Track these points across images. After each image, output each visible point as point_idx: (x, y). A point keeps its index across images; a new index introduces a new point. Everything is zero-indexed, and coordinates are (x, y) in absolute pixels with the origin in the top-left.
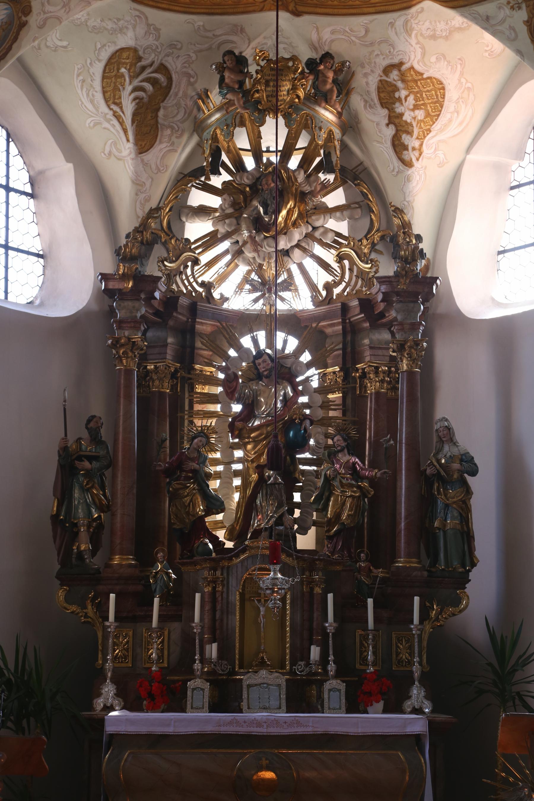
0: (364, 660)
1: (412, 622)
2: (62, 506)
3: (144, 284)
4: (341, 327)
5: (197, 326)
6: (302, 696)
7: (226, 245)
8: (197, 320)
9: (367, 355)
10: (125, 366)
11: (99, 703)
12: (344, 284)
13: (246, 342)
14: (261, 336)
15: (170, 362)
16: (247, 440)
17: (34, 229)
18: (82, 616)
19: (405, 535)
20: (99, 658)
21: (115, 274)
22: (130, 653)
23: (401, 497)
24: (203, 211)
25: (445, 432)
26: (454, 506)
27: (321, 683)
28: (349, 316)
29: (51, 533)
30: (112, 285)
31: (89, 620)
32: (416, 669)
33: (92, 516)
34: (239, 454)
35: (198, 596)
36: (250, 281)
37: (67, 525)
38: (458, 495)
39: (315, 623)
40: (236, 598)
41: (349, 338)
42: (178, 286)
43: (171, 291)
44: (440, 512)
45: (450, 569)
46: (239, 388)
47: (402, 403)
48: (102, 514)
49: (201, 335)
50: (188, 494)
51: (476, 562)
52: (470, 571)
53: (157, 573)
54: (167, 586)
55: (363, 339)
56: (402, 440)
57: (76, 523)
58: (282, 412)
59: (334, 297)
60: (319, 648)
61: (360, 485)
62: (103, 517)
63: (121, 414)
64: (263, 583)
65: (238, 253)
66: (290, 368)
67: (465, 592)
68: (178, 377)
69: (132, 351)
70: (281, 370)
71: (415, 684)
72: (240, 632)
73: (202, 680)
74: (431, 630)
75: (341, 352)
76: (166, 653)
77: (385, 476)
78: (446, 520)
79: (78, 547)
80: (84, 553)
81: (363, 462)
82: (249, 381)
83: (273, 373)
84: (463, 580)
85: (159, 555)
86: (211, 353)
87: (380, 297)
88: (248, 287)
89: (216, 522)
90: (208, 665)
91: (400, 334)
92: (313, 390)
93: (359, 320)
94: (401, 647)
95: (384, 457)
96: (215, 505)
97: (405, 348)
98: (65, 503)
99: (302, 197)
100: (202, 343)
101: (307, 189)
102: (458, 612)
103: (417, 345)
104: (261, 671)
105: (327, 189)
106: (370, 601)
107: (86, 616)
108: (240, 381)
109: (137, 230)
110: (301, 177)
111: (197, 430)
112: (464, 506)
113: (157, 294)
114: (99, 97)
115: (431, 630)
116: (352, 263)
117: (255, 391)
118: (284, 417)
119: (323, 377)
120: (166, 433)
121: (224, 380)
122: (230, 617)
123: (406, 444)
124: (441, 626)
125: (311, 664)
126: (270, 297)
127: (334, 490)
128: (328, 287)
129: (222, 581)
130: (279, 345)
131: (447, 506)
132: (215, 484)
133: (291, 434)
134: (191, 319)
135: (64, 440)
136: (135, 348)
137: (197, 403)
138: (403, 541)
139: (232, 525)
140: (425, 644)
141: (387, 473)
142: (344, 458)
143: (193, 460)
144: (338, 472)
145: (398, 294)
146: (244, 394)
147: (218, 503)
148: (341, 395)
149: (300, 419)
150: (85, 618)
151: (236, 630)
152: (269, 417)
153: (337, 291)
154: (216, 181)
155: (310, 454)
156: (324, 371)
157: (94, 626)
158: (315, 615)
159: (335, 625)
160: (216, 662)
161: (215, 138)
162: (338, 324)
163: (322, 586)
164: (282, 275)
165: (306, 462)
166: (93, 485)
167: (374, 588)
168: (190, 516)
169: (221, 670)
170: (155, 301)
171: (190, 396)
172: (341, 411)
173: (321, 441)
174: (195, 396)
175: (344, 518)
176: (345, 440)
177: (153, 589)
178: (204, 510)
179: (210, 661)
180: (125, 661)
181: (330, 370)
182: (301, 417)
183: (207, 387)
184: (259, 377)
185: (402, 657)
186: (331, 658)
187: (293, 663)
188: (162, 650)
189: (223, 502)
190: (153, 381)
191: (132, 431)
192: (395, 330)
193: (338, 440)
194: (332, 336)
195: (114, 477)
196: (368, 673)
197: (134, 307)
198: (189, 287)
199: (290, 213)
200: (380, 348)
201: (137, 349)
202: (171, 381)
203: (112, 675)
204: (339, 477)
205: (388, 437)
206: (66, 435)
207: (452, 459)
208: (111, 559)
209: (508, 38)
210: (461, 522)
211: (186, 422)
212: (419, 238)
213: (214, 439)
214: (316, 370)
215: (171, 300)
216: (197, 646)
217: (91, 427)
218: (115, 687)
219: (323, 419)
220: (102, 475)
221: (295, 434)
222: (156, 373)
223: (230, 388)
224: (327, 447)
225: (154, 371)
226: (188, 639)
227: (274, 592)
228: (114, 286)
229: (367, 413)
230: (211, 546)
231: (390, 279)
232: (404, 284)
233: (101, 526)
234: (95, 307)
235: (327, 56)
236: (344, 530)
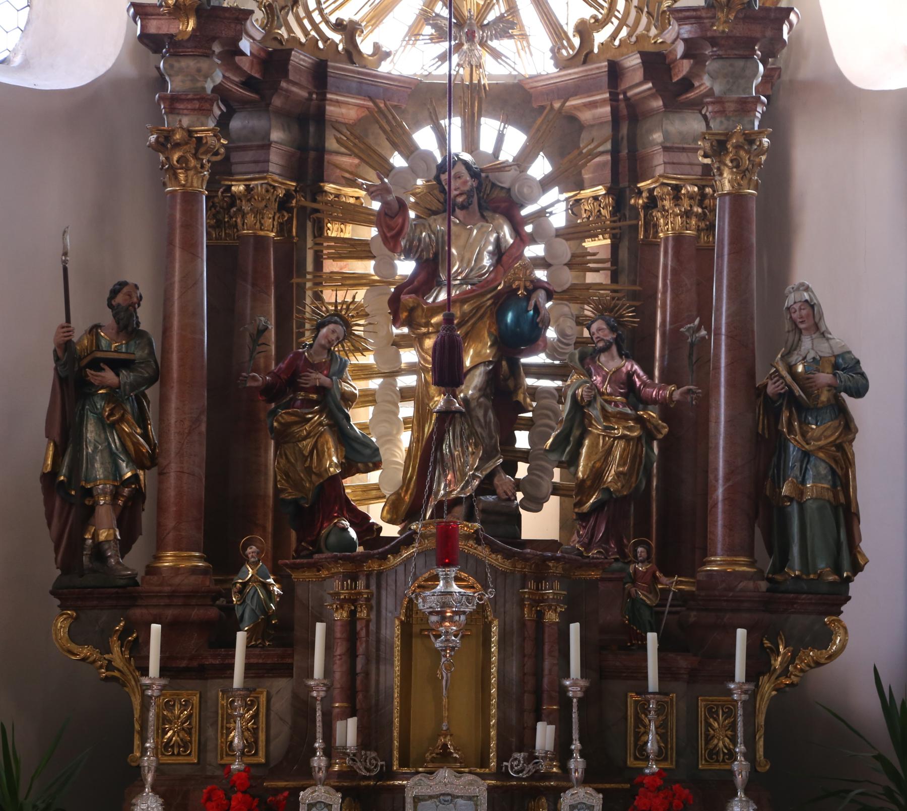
0: (641, 748)
1: (732, 678)
2: (63, 456)
4: (608, 109)
5: (328, 107)
8: (329, 96)
9: (659, 161)
10: (184, 186)
12: (616, 22)
14: (455, 126)
15: (277, 177)
16: (424, 330)
18: (101, 667)
19: (724, 512)
20: (135, 747)
21: (161, 6)
22: (195, 738)
23: (717, 439)
25: (804, 312)
26: (821, 455)
28: (623, 87)
29: (42, 509)
30: (154, 27)
31: (116, 674)
32: (740, 768)
33: (121, 476)
34: (409, 356)
35: (320, 629)
36: (434, 18)
37: (73, 493)
38: (829, 432)
39: (546, 680)
40: (393, 632)
41: (624, 130)
42: (290, 30)
43: (276, 39)
44: (793, 468)
45: (812, 576)
46: (407, 229)
47: (721, 256)
48: (141, 473)
49: (337, 125)
50: (309, 433)
51: (862, 563)
52: (849, 580)
53: (245, 585)
54: (265, 610)
55: (651, 131)
56: (720, 329)
57: (91, 489)
58: (492, 276)
59: (596, 50)
60: (553, 727)
61: (641, 416)
62: (142, 477)
63: (177, 278)
64: (424, 602)
66: (509, 190)
67: (840, 621)
68: (292, 208)
69: (195, 156)
70: (490, 194)
71: (736, 795)
72: (401, 697)
73: (328, 787)
74: (774, 693)
75: (608, 158)
76: (262, 737)
77: (689, 399)
78: (803, 482)
79: (95, 536)
80: (106, 546)
81: (650, 373)
82: (430, 216)
83: (475, 200)
84: (837, 597)
85: (249, 550)
86: (356, 161)
87: (680, 48)
88: (428, 30)
89: (367, 488)
90: (340, 758)
91: (718, 120)
92: (553, 233)
93: (643, 95)
94: (716, 725)
95: (688, 360)
96: (359, 454)
97: (727, 149)
98: (69, 450)
100: (339, 141)
102: (827, 659)
103: (751, 142)
104: (441, 771)
106: (652, 638)
107: (110, 666)
108: (412, 214)
111: (327, 310)
112: (839, 454)
113: (245, 45)
115: (774, 693)
117: (440, 235)
118: (497, 283)
119: (575, 206)
120: (266, 314)
121: (379, 212)
122: (382, 668)
123: (727, 337)
124: (792, 685)
125: (537, 758)
126: (471, 51)
127: (591, 425)
128: (585, 30)
129: (368, 600)
130: (486, 145)
131: (806, 455)
132: (360, 416)
133: (510, 317)
134: (317, 94)
135: (65, 330)
136: (202, 150)
137: (329, 258)
138: (720, 523)
139: (397, 494)
140: (761, 719)
141: (694, 393)
142: (611, 363)
143: (318, 367)
144: (599, 390)
145: (713, 41)
146: (420, 240)
147: (368, 452)
148: (608, 241)
149: (526, 289)
150: (107, 670)
151: (393, 692)
152: (467, 284)
153: (600, 37)
155: (548, 356)
156: (575, 195)
157: (124, 685)
158: (547, 664)
159: (584, 683)
160: (354, 755)
162: (603, 102)
163: (559, 609)
164: (496, 7)
165: (541, 371)
166: (123, 415)
167: (663, 613)
168: (314, 477)
169: (365, 768)
170: (243, 58)
171: (316, 244)
172: (609, 272)
173: (569, 332)
174: (325, 244)
175: (610, 479)
176: (612, 329)
177: (238, 615)
178: (341, 465)
179: (343, 752)
180: (185, 751)
181: (587, 193)
182: (528, 284)
183: (350, 227)
185: (717, 745)
186: (576, 745)
187: (503, 756)
188: (255, 731)
189: (377, 450)
190: (244, 216)
191: (197, 313)
192: (708, 114)
193: (599, 330)
194: (592, 126)
195: (163, 400)
196: (646, 775)
197: (199, 70)
198: (313, 33)
200: (683, 150)
201: (206, 153)
202: (277, 215)
203: (155, 780)
204: (599, 400)
205: (697, 321)
206: (68, 319)
207: (817, 363)
208: (158, 558)
210: (834, 486)
211: (309, 293)
213: (362, 328)
214: (561, 192)
215: (275, 59)
216: (319, 724)
217: (119, 305)
218: (160, 801)
219: (573, 288)
220: (140, 398)
221: (517, 319)
222: (249, 201)
223: (391, 229)
224: (580, 342)
225: (245, 196)
226: (303, 707)
227: (444, 619)
228: (159, 28)
229: (657, 277)
230: (353, 533)
231: (699, 13)
232: (725, 22)
233: (138, 496)
234: (130, 70)
236: (611, 505)
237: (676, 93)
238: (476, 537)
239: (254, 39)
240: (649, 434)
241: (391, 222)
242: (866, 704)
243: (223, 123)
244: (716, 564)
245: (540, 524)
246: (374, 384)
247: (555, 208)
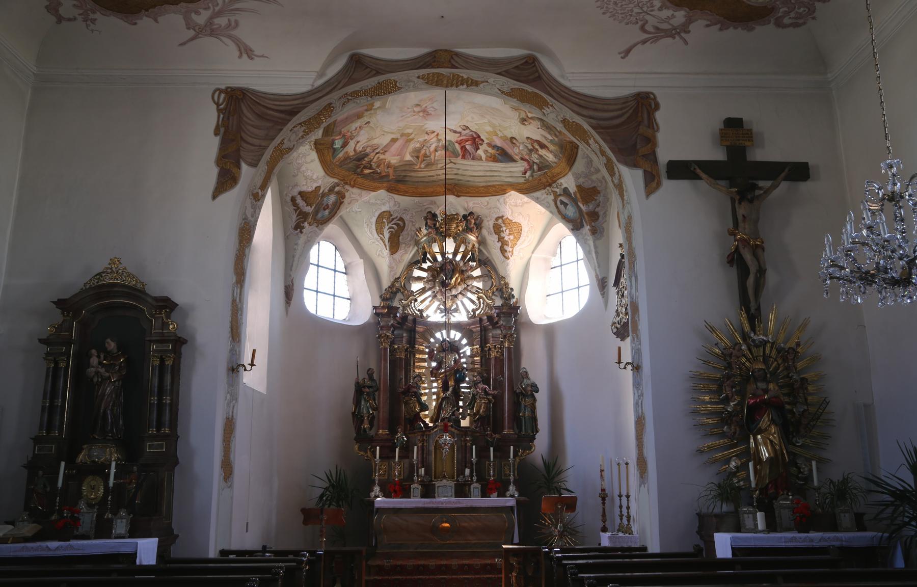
3: (392, 310)
6: (461, 491)
7: (429, 293)
11: (373, 494)
13: (438, 335)
14: (444, 332)
17: (347, 288)
24: (419, 279)
27: (470, 485)
30: (378, 311)
32: (512, 478)
34: (435, 384)
65: (435, 297)
70: (453, 347)
95: (499, 385)
96: (424, 407)
99: (462, 272)
101: (464, 269)
105: (473, 269)
109: (389, 287)
110: (462, 264)
114: (374, 231)
116: (484, 300)
128: (474, 311)
130: (452, 336)
132: (424, 398)
142: (481, 386)
153: (477, 312)
154: (425, 266)
161: (424, 248)
165: (465, 388)
184: (444, 350)
187: (458, 476)
199: (457, 279)
207: (528, 385)
209: (547, 207)
212: (512, 289)
215: (405, 317)
226: (412, 466)
233: (373, 417)
234: (372, 321)
235: (471, 213)
236: (481, 418)
237: (495, 325)
238: (452, 426)
239: (754, 317)
240: (490, 401)
241: (431, 357)
242: (539, 462)
243: (393, 332)
244: (506, 431)
245: (465, 423)
246: (427, 391)
247: (468, 350)
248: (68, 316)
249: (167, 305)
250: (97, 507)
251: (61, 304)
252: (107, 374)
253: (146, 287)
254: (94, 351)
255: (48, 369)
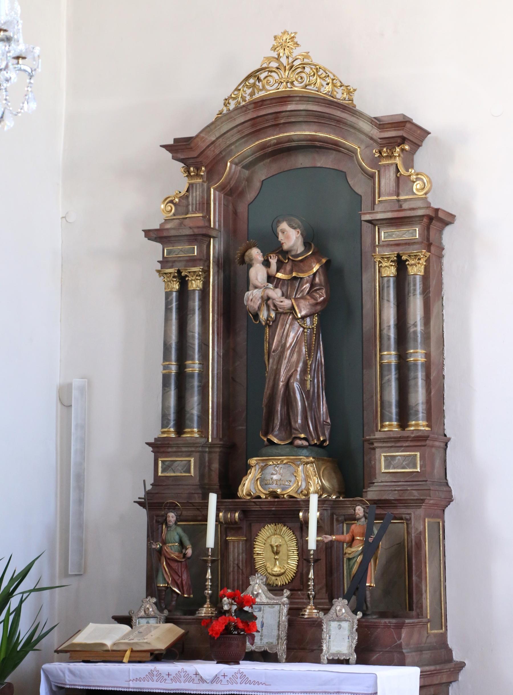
248: (197, 175)
249: (403, 135)
250: (287, 593)
251: (180, 148)
252: (287, 303)
253: (356, 98)
254: (256, 253)
255: (168, 295)
